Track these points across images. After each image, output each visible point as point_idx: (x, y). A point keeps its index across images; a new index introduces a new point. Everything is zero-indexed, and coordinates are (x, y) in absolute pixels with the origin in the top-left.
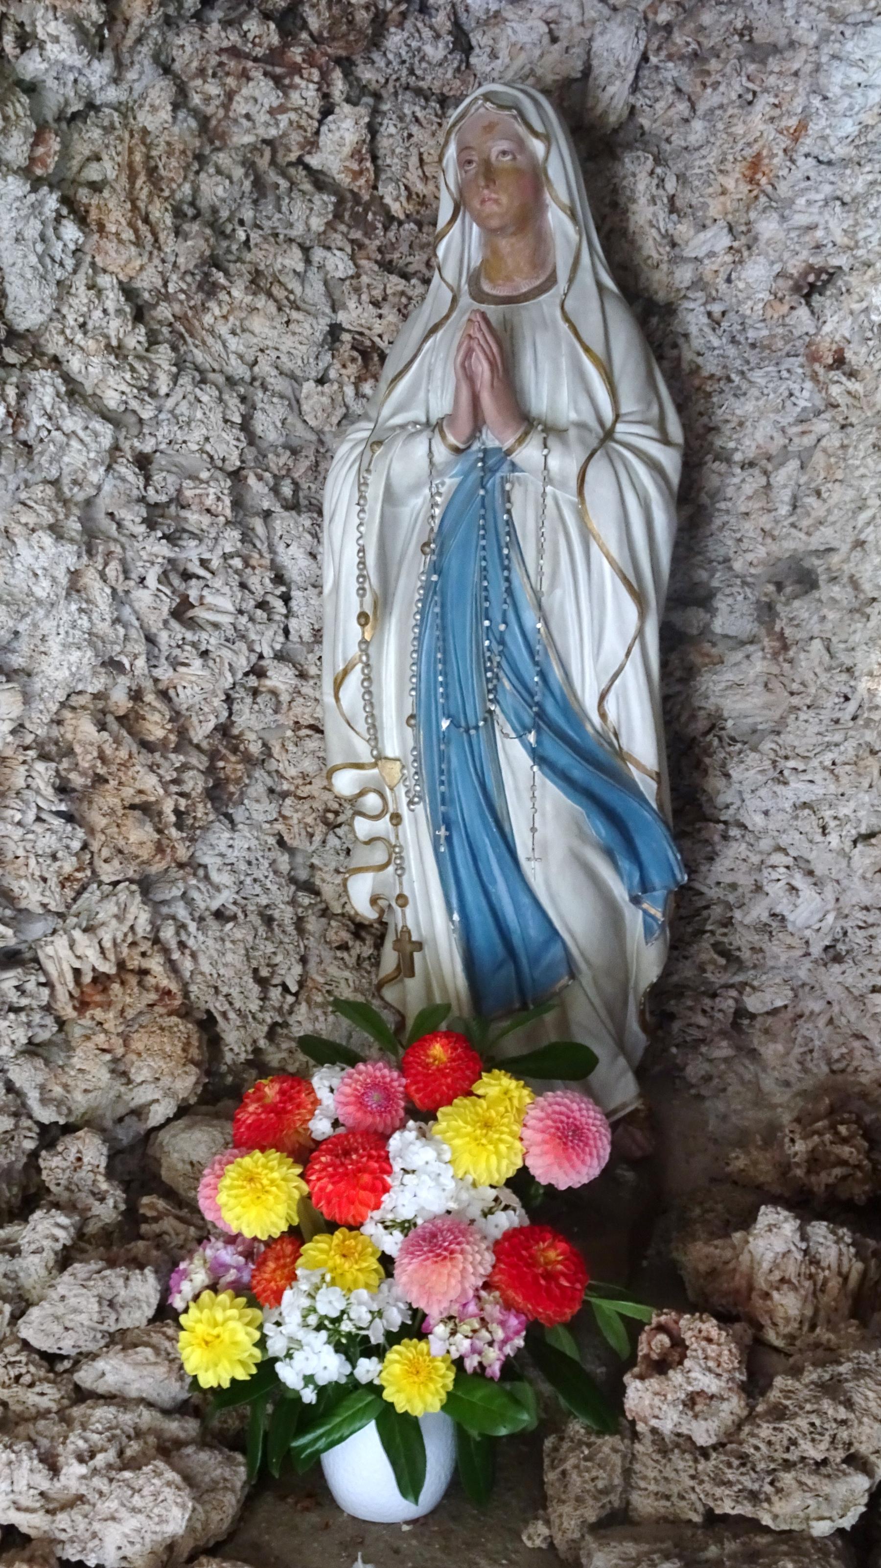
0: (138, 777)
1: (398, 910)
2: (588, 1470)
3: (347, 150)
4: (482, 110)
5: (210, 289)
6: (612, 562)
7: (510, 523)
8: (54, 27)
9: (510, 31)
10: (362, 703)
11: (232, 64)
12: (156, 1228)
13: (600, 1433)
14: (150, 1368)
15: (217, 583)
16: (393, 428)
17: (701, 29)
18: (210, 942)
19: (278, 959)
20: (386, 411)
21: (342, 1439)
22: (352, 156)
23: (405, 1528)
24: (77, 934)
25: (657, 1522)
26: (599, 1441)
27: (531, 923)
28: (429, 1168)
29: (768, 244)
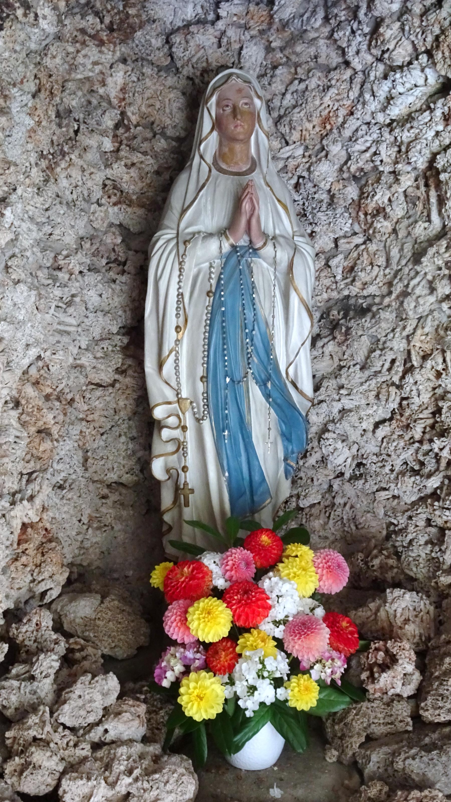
0: (45, 415)
1: (183, 474)
2: (358, 719)
3: (119, 88)
4: (233, 81)
5: (63, 154)
6: (302, 300)
7: (253, 282)
8: (47, 11)
9: (197, 39)
10: (175, 371)
11: (80, 37)
12: (84, 654)
13: (356, 702)
14: (132, 723)
15: (71, 310)
16: (194, 234)
17: (294, 53)
18: (58, 501)
19: (83, 506)
20: (182, 225)
21: (258, 731)
22: (121, 90)
23: (276, 768)
24: (25, 502)
25: (386, 736)
26: (359, 706)
27: (257, 474)
28: (289, 593)
29: (334, 156)
